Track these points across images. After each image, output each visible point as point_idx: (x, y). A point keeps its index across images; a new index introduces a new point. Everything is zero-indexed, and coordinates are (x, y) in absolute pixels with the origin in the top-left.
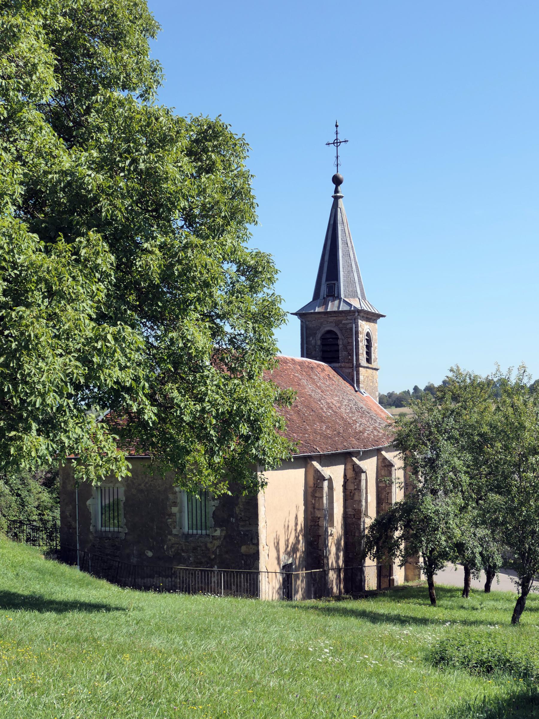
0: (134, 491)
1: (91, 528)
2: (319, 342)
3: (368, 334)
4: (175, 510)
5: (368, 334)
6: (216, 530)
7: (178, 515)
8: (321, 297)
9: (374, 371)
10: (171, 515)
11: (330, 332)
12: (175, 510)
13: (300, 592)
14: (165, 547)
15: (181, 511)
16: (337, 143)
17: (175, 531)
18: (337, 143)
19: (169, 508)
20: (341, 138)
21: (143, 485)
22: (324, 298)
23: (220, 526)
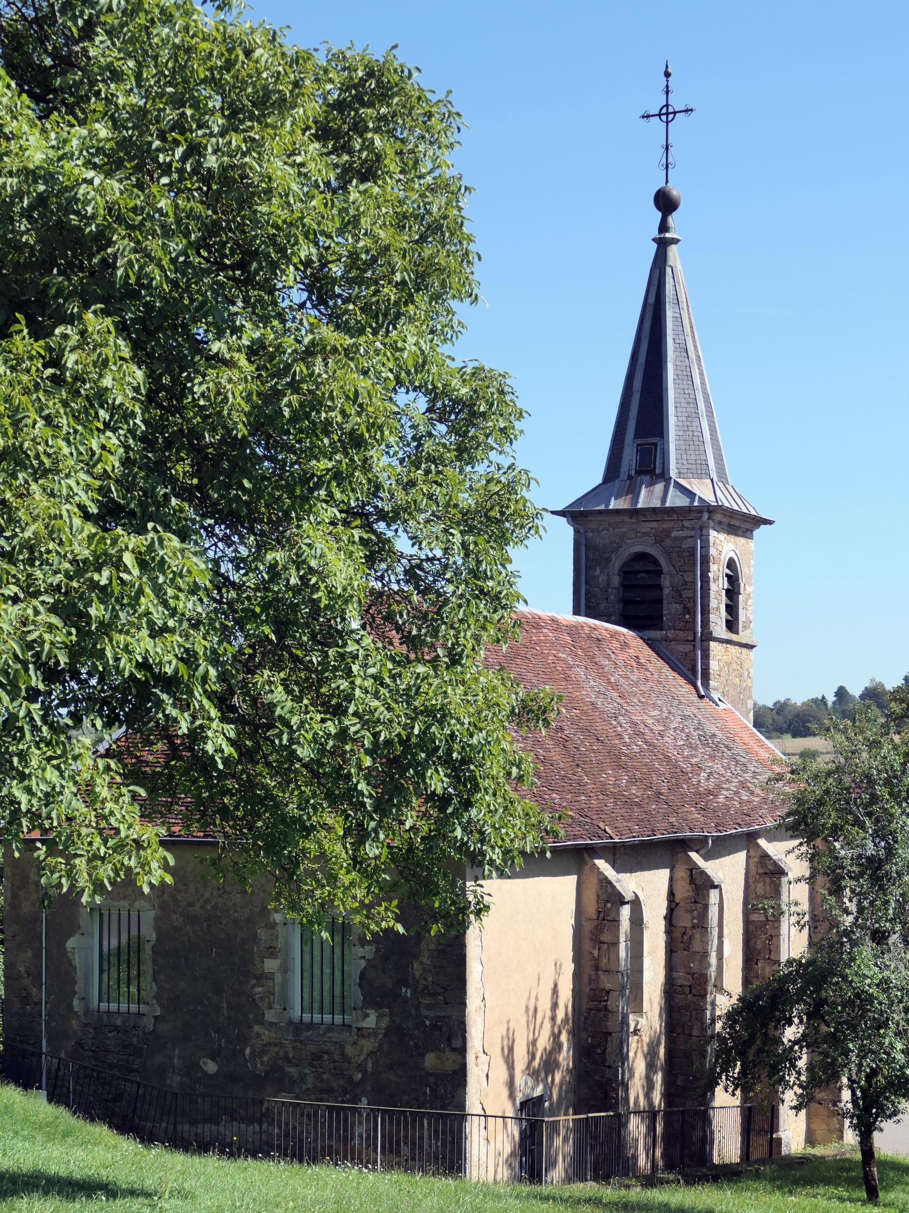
0: (177, 920)
1: (76, 1002)
2: (616, 581)
3: (731, 564)
4: (271, 965)
5: (731, 564)
6: (366, 1015)
7: (278, 978)
8: (623, 475)
9: (745, 651)
11: (642, 557)
12: (271, 965)
14: (248, 1051)
15: (285, 969)
16: (666, 114)
17: (270, 1016)
18: (666, 114)
19: (257, 961)
20: (676, 103)
22: (630, 477)
23: (377, 1006)
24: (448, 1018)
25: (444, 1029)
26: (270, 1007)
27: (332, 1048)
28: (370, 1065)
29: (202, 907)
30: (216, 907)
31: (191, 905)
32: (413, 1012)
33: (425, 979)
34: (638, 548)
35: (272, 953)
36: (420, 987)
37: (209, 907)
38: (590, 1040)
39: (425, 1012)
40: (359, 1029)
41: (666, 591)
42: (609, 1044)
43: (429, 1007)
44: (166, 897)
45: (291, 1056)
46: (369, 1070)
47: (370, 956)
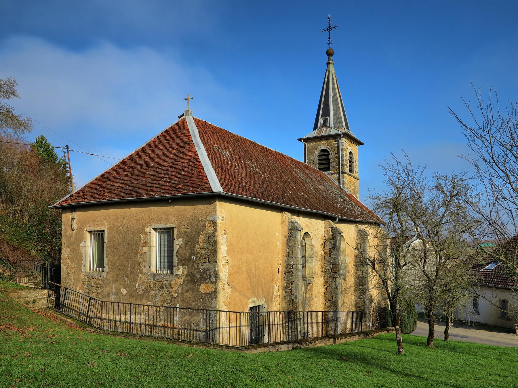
0: (115, 233)
1: (82, 267)
2: (317, 158)
3: (351, 153)
4: (145, 249)
5: (351, 153)
6: (179, 269)
7: (148, 253)
8: (318, 128)
9: (356, 180)
10: (143, 254)
11: (323, 151)
12: (145, 249)
13: (381, 333)
14: (137, 285)
15: (150, 251)
16: (329, 29)
17: (145, 270)
18: (329, 29)
19: (140, 248)
20: (332, 25)
21: (121, 228)
22: (320, 128)
23: (183, 265)
24: (210, 269)
25: (208, 273)
26: (145, 267)
27: (167, 283)
28: (180, 290)
29: (123, 228)
30: (127, 227)
31: (119, 227)
32: (196, 267)
33: (201, 252)
34: (322, 148)
35: (146, 245)
36: (199, 256)
37: (125, 227)
38: (286, 284)
39: (200, 266)
40: (176, 275)
41: (331, 160)
42: (313, 292)
43: (202, 265)
44: (111, 225)
45: (152, 286)
46: (180, 292)
47: (180, 244)
